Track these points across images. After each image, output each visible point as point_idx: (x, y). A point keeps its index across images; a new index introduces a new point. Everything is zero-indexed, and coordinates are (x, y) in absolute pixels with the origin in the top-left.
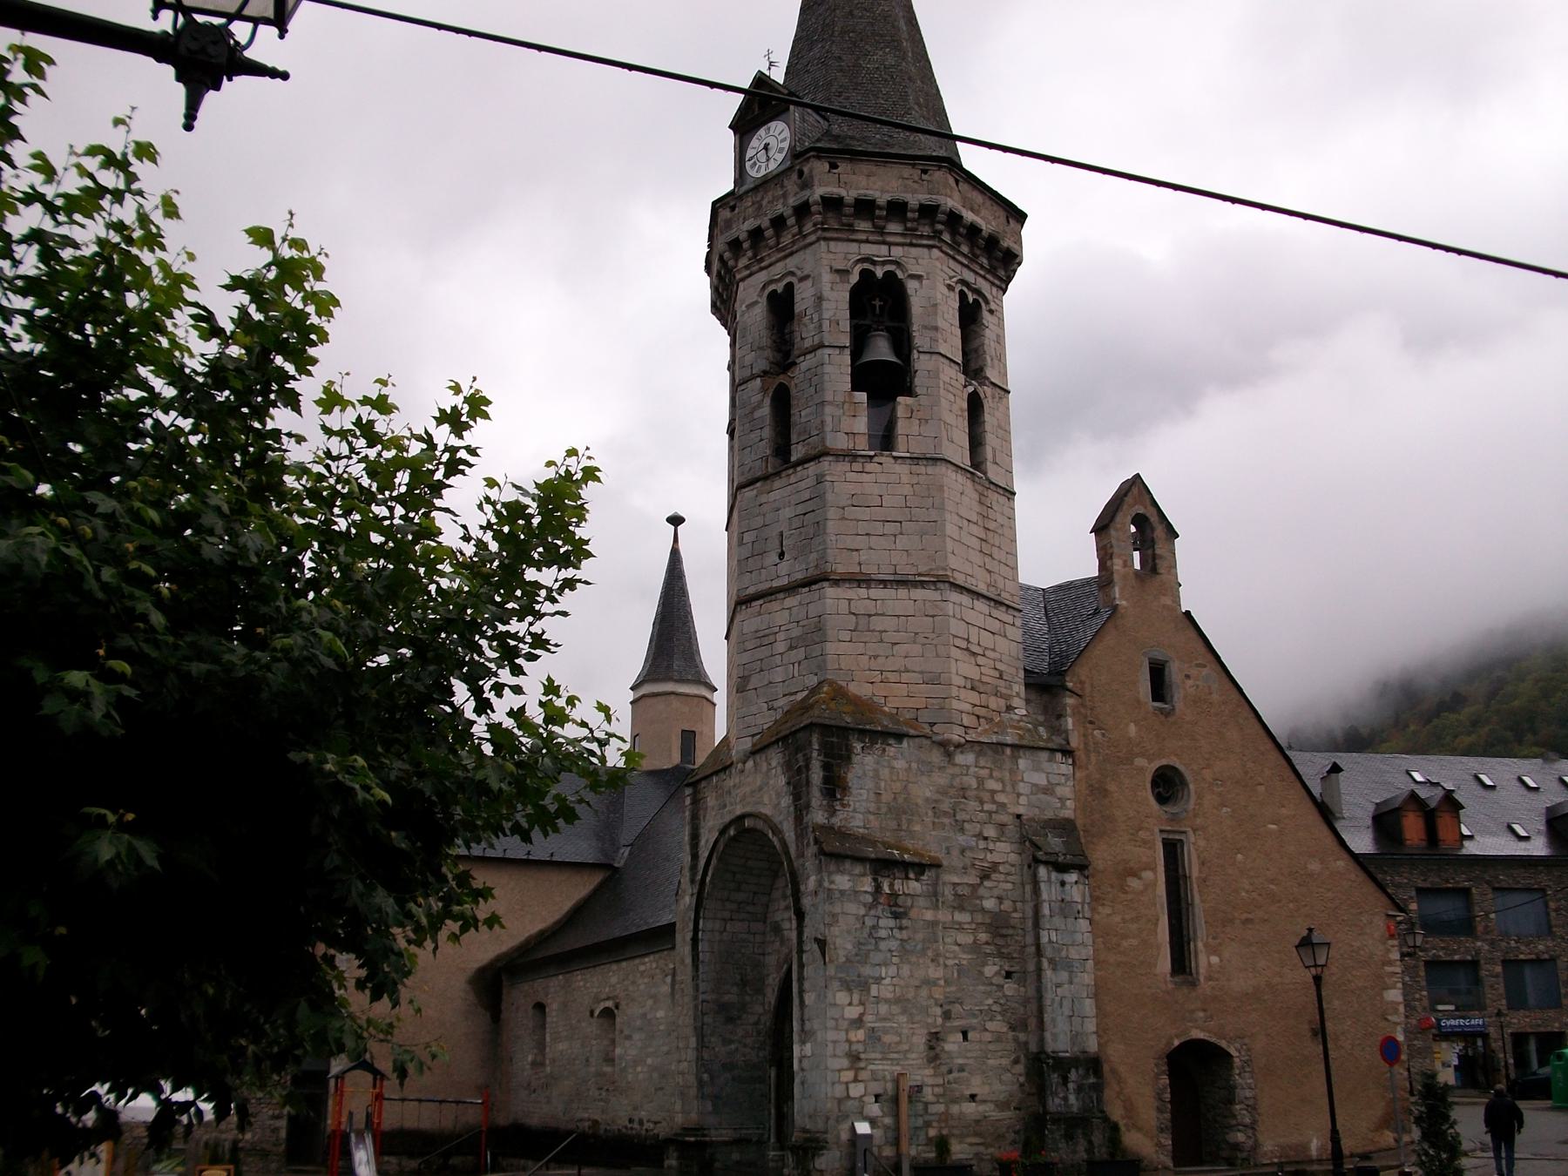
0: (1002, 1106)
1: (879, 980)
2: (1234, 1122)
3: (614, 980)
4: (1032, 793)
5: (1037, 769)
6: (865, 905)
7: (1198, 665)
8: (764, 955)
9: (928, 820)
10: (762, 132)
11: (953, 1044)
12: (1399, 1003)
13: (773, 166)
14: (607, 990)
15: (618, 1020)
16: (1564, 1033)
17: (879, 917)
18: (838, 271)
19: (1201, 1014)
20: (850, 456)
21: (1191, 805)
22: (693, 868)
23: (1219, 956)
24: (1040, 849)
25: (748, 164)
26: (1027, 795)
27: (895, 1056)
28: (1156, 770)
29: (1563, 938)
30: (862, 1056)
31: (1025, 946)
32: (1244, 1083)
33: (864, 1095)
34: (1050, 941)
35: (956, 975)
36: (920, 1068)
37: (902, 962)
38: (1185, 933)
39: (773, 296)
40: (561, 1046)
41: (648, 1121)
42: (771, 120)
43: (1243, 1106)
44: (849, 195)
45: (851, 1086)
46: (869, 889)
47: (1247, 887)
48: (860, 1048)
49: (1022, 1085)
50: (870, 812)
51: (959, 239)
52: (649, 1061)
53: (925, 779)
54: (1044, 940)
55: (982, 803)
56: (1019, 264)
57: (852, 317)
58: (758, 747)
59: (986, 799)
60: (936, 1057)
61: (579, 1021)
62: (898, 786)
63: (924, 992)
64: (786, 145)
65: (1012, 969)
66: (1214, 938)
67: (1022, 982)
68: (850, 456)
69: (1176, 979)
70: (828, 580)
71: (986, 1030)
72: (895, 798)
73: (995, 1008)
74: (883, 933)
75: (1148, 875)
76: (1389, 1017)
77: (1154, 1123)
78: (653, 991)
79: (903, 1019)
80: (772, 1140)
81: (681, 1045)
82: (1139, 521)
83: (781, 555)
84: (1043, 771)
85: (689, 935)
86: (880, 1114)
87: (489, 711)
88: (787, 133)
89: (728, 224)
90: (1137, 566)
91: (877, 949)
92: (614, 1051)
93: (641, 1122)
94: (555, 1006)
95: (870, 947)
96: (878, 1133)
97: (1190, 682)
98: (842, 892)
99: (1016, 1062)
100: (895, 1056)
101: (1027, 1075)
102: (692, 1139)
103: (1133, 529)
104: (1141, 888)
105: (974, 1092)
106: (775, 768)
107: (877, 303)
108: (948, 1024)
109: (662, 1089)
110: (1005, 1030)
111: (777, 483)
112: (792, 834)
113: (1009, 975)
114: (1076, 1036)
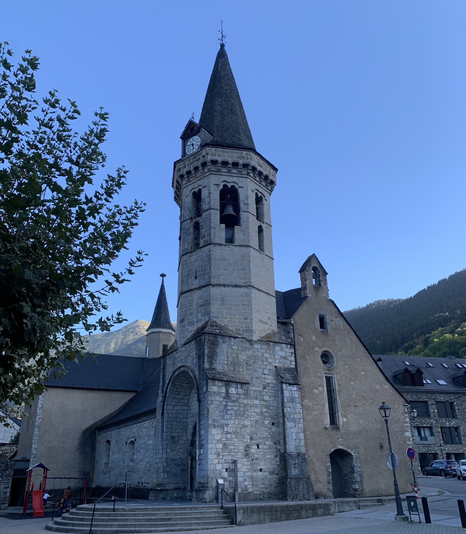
0: (272, 473)
2: (354, 481)
3: (135, 430)
4: (280, 359)
5: (282, 350)
7: (335, 317)
8: (187, 418)
9: (245, 367)
10: (191, 140)
11: (254, 449)
13: (195, 150)
14: (132, 434)
15: (136, 445)
16: (464, 453)
17: (227, 402)
18: (216, 185)
19: (341, 439)
20: (221, 245)
21: (335, 365)
23: (346, 418)
24: (283, 378)
25: (187, 151)
26: (278, 359)
27: (233, 454)
28: (323, 352)
29: (461, 419)
30: (221, 454)
31: (279, 413)
32: (356, 464)
35: (255, 424)
36: (242, 459)
38: (334, 410)
39: (194, 193)
40: (115, 456)
42: (195, 135)
43: (357, 474)
44: (220, 159)
45: (217, 465)
46: (224, 392)
49: (278, 465)
51: (256, 176)
52: (146, 460)
53: (243, 353)
54: (285, 411)
55: (263, 361)
56: (275, 185)
57: (220, 200)
58: (186, 343)
59: (264, 360)
60: (248, 454)
61: (122, 446)
63: (243, 430)
64: (199, 144)
65: (274, 422)
66: (344, 412)
67: (278, 427)
68: (221, 245)
69: (332, 426)
70: (211, 285)
71: (265, 444)
72: (233, 359)
74: (229, 408)
75: (320, 388)
76: (407, 442)
77: (326, 480)
78: (148, 434)
80: (189, 488)
82: (315, 269)
83: (196, 277)
85: (161, 411)
86: (227, 476)
87: (16, 73)
88: (199, 140)
89: (179, 170)
90: (314, 284)
91: (227, 414)
92: (134, 457)
94: (114, 441)
96: (227, 484)
97: (332, 323)
98: (215, 393)
99: (276, 456)
100: (233, 454)
102: (160, 488)
103: (313, 272)
104: (318, 393)
105: (261, 468)
107: (229, 196)
109: (150, 470)
110: (272, 444)
111: (194, 254)
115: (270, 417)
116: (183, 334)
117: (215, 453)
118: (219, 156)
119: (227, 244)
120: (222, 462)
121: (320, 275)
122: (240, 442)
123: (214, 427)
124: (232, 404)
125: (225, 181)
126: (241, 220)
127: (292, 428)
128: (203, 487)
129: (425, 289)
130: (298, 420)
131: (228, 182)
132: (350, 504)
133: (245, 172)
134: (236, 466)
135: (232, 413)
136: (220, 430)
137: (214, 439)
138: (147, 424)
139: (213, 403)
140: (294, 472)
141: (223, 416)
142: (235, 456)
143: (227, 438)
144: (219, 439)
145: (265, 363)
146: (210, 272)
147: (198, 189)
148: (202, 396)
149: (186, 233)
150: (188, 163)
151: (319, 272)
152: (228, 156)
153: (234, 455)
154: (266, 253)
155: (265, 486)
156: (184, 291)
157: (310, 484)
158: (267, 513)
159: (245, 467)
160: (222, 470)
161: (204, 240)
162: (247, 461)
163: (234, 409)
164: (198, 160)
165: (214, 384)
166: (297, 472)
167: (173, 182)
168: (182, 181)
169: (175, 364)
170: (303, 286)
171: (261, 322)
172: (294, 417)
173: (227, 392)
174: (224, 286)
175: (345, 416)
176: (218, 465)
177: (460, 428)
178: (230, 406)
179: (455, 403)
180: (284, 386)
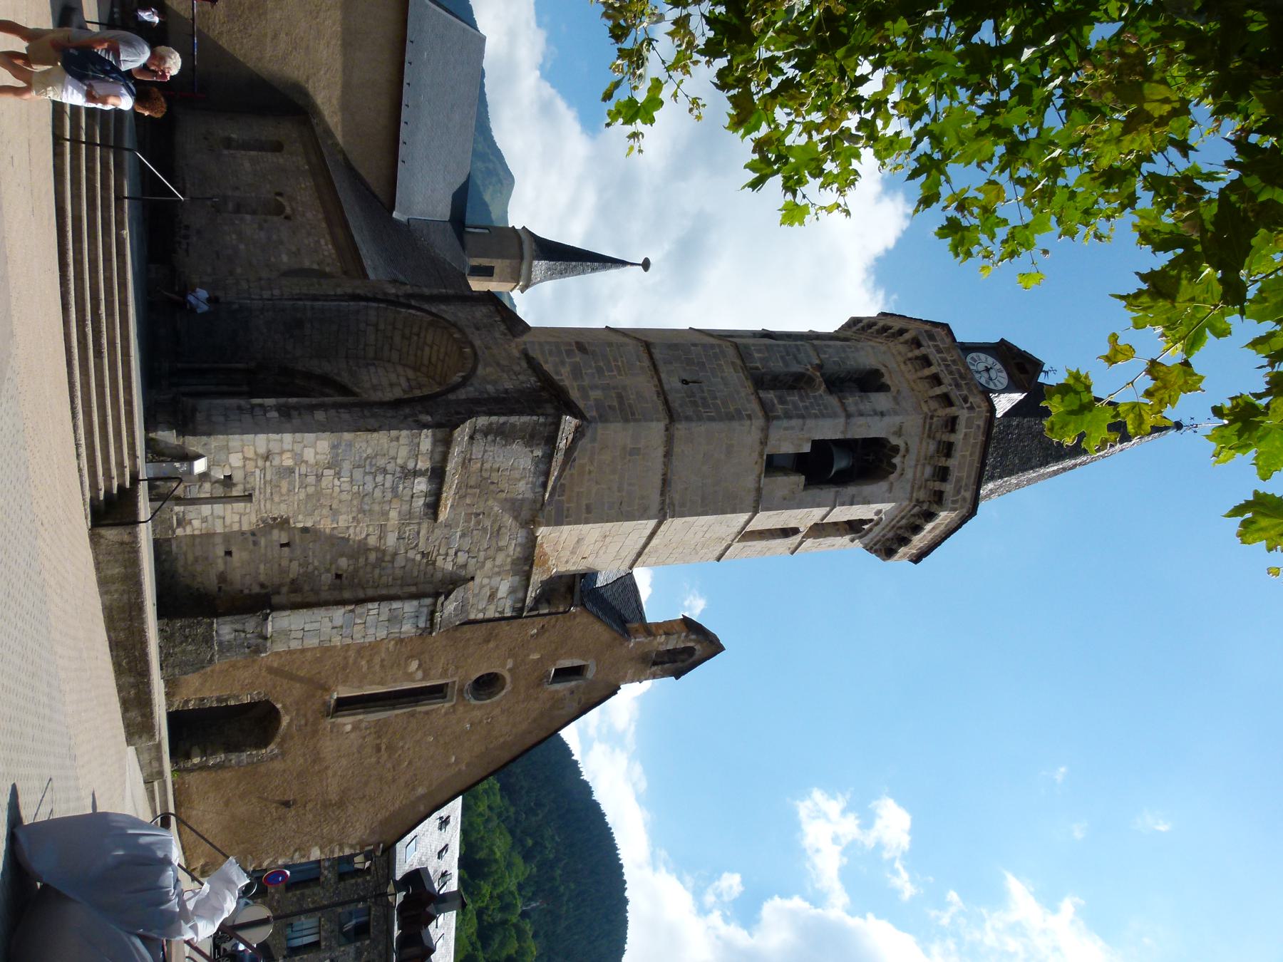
0: (222, 578)
1: (338, 475)
6: (405, 463)
7: (580, 699)
12: (309, 858)
15: (275, 219)
17: (394, 474)
20: (764, 442)
22: (422, 297)
24: (446, 598)
25: (974, 355)
29: (337, 888)
30: (268, 464)
31: (363, 588)
33: (231, 467)
38: (371, 704)
40: (247, 165)
41: (188, 244)
44: (958, 438)
45: (240, 455)
46: (418, 467)
47: (407, 747)
49: (242, 591)
50: (482, 464)
54: (370, 606)
55: (486, 550)
63: (325, 511)
65: (344, 579)
67: (332, 587)
68: (764, 442)
71: (291, 561)
73: (311, 568)
74: (379, 478)
75: (420, 674)
76: (297, 853)
79: (302, 496)
80: (179, 365)
81: (263, 282)
82: (689, 651)
83: (685, 382)
84: (508, 595)
89: (931, 337)
91: (366, 473)
92: (247, 213)
93: (186, 237)
94: (281, 161)
95: (367, 467)
99: (262, 586)
100: (269, 491)
101: (250, 595)
105: (234, 554)
106: (518, 379)
108: (296, 532)
110: (291, 576)
112: (464, 397)
113: (338, 576)
115: (356, 570)
116: (551, 353)
119: (765, 457)
120: (247, 467)
121: (676, 664)
122: (296, 506)
123: (334, 447)
124: (388, 485)
125: (907, 450)
126: (818, 490)
128: (185, 425)
129: (573, 755)
131: (904, 456)
132: (155, 764)
133: (922, 495)
134: (238, 499)
135: (366, 487)
137: (305, 447)
138: (325, 247)
139: (392, 441)
140: (225, 629)
141: (359, 467)
142: (262, 496)
143: (306, 476)
144: (305, 459)
145: (482, 554)
146: (700, 419)
147: (889, 382)
148: (407, 411)
149: (788, 354)
150: (949, 358)
151: (683, 661)
152: (964, 456)
153: (265, 492)
155: (189, 562)
156: (653, 350)
158: (126, 597)
159: (236, 518)
160: (227, 466)
161: (776, 402)
162: (250, 523)
163: (377, 490)
164: (958, 386)
165: (438, 444)
166: (227, 637)
167: (895, 315)
168: (906, 342)
169: (478, 329)
170: (654, 629)
171: (578, 542)
173: (416, 473)
174: (668, 454)
175: (356, 727)
176: (241, 457)
177: (319, 888)
178: (384, 480)
179: (368, 878)
180: (428, 601)
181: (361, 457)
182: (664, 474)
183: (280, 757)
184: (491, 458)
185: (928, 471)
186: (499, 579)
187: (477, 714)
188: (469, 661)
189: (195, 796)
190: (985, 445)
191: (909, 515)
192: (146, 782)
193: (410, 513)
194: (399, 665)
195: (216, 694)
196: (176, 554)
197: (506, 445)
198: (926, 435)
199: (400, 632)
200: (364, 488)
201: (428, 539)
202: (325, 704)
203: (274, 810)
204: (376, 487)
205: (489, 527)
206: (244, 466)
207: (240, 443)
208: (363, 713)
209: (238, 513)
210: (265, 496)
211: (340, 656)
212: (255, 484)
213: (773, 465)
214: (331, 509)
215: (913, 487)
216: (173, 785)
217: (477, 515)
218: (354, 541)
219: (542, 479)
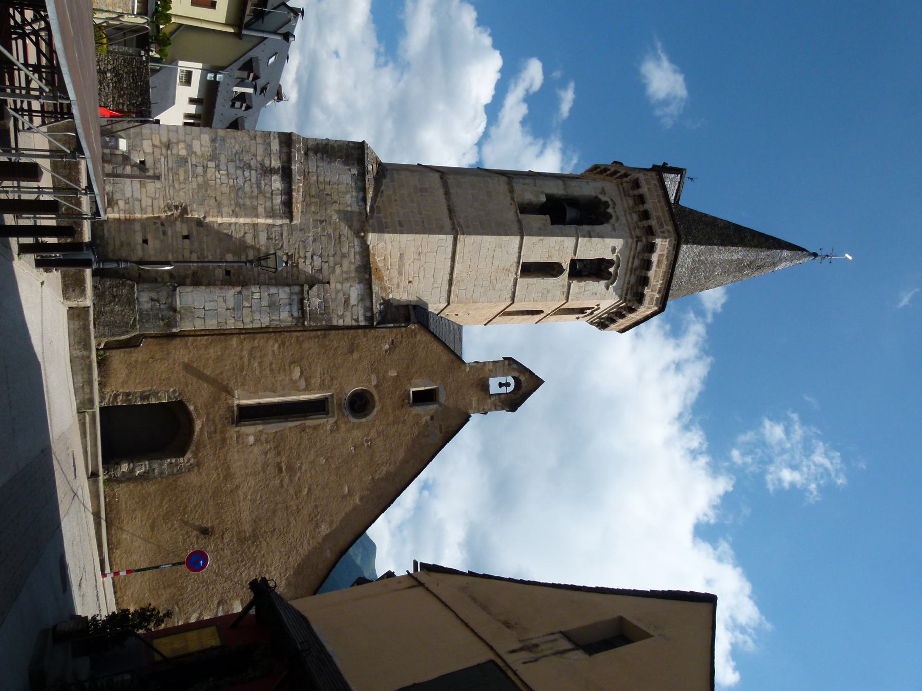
6: (263, 160)
7: (440, 426)
23: (254, 444)
26: (342, 289)
30: (169, 152)
33: (144, 152)
34: (253, 293)
37: (230, 187)
44: (644, 190)
46: (272, 165)
48: (175, 151)
50: (318, 177)
62: (335, 198)
63: (212, 202)
65: (232, 275)
69: (235, 408)
74: (247, 174)
75: (302, 384)
76: (221, 608)
84: (358, 302)
95: (238, 162)
100: (171, 178)
105: (149, 242)
114: (191, 312)
117: (169, 140)
118: (649, 189)
122: (191, 194)
123: (213, 141)
124: (253, 180)
125: (614, 204)
127: (225, 301)
130: (240, 317)
131: (614, 208)
135: (238, 180)
136: (208, 151)
137: (193, 139)
139: (251, 140)
141: (232, 161)
143: (196, 166)
154: (520, 281)
155: (117, 248)
157: (124, 329)
163: (246, 185)
172: (244, 307)
173: (271, 171)
174: (447, 193)
178: (250, 175)
181: (232, 152)
182: (448, 206)
183: (196, 468)
184: (322, 173)
185: (635, 217)
186: (348, 285)
187: (357, 433)
188: (341, 371)
189: (124, 515)
190: (676, 231)
191: (637, 254)
192: (79, 412)
193: (272, 210)
194: (285, 370)
195: (139, 390)
196: (107, 238)
197: (330, 162)
198: (623, 195)
199: (280, 320)
200: (237, 182)
201: (289, 241)
202: (230, 408)
203: (194, 540)
204: (245, 181)
205: (332, 234)
206: (153, 153)
207: (150, 131)
208: (263, 424)
209: (151, 197)
210: (168, 182)
211: (236, 355)
212: (161, 171)
213: (526, 209)
214: (216, 201)
215: (630, 229)
216: (105, 498)
217: (321, 222)
218: (236, 238)
219: (361, 195)
